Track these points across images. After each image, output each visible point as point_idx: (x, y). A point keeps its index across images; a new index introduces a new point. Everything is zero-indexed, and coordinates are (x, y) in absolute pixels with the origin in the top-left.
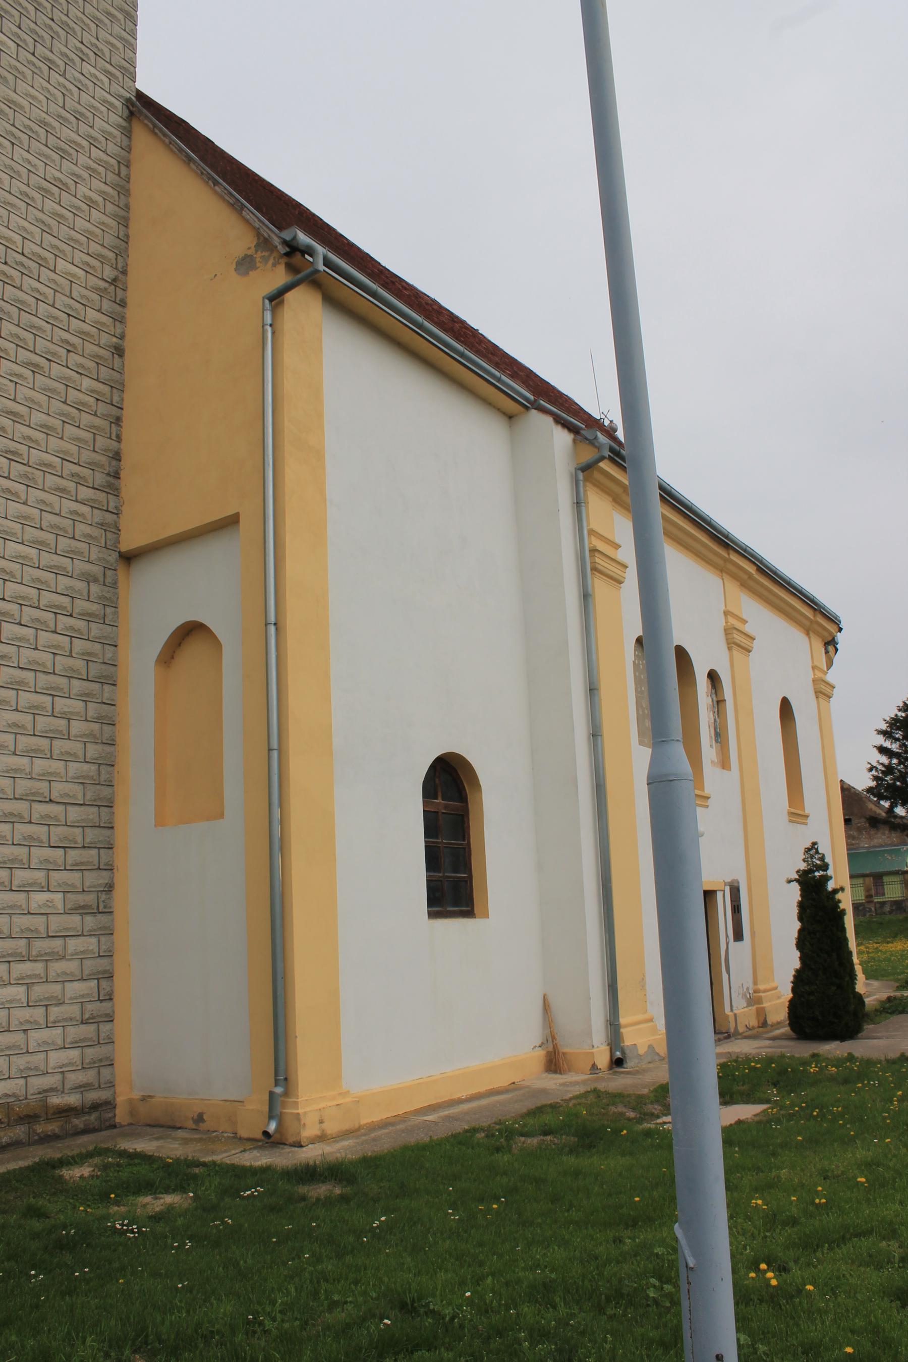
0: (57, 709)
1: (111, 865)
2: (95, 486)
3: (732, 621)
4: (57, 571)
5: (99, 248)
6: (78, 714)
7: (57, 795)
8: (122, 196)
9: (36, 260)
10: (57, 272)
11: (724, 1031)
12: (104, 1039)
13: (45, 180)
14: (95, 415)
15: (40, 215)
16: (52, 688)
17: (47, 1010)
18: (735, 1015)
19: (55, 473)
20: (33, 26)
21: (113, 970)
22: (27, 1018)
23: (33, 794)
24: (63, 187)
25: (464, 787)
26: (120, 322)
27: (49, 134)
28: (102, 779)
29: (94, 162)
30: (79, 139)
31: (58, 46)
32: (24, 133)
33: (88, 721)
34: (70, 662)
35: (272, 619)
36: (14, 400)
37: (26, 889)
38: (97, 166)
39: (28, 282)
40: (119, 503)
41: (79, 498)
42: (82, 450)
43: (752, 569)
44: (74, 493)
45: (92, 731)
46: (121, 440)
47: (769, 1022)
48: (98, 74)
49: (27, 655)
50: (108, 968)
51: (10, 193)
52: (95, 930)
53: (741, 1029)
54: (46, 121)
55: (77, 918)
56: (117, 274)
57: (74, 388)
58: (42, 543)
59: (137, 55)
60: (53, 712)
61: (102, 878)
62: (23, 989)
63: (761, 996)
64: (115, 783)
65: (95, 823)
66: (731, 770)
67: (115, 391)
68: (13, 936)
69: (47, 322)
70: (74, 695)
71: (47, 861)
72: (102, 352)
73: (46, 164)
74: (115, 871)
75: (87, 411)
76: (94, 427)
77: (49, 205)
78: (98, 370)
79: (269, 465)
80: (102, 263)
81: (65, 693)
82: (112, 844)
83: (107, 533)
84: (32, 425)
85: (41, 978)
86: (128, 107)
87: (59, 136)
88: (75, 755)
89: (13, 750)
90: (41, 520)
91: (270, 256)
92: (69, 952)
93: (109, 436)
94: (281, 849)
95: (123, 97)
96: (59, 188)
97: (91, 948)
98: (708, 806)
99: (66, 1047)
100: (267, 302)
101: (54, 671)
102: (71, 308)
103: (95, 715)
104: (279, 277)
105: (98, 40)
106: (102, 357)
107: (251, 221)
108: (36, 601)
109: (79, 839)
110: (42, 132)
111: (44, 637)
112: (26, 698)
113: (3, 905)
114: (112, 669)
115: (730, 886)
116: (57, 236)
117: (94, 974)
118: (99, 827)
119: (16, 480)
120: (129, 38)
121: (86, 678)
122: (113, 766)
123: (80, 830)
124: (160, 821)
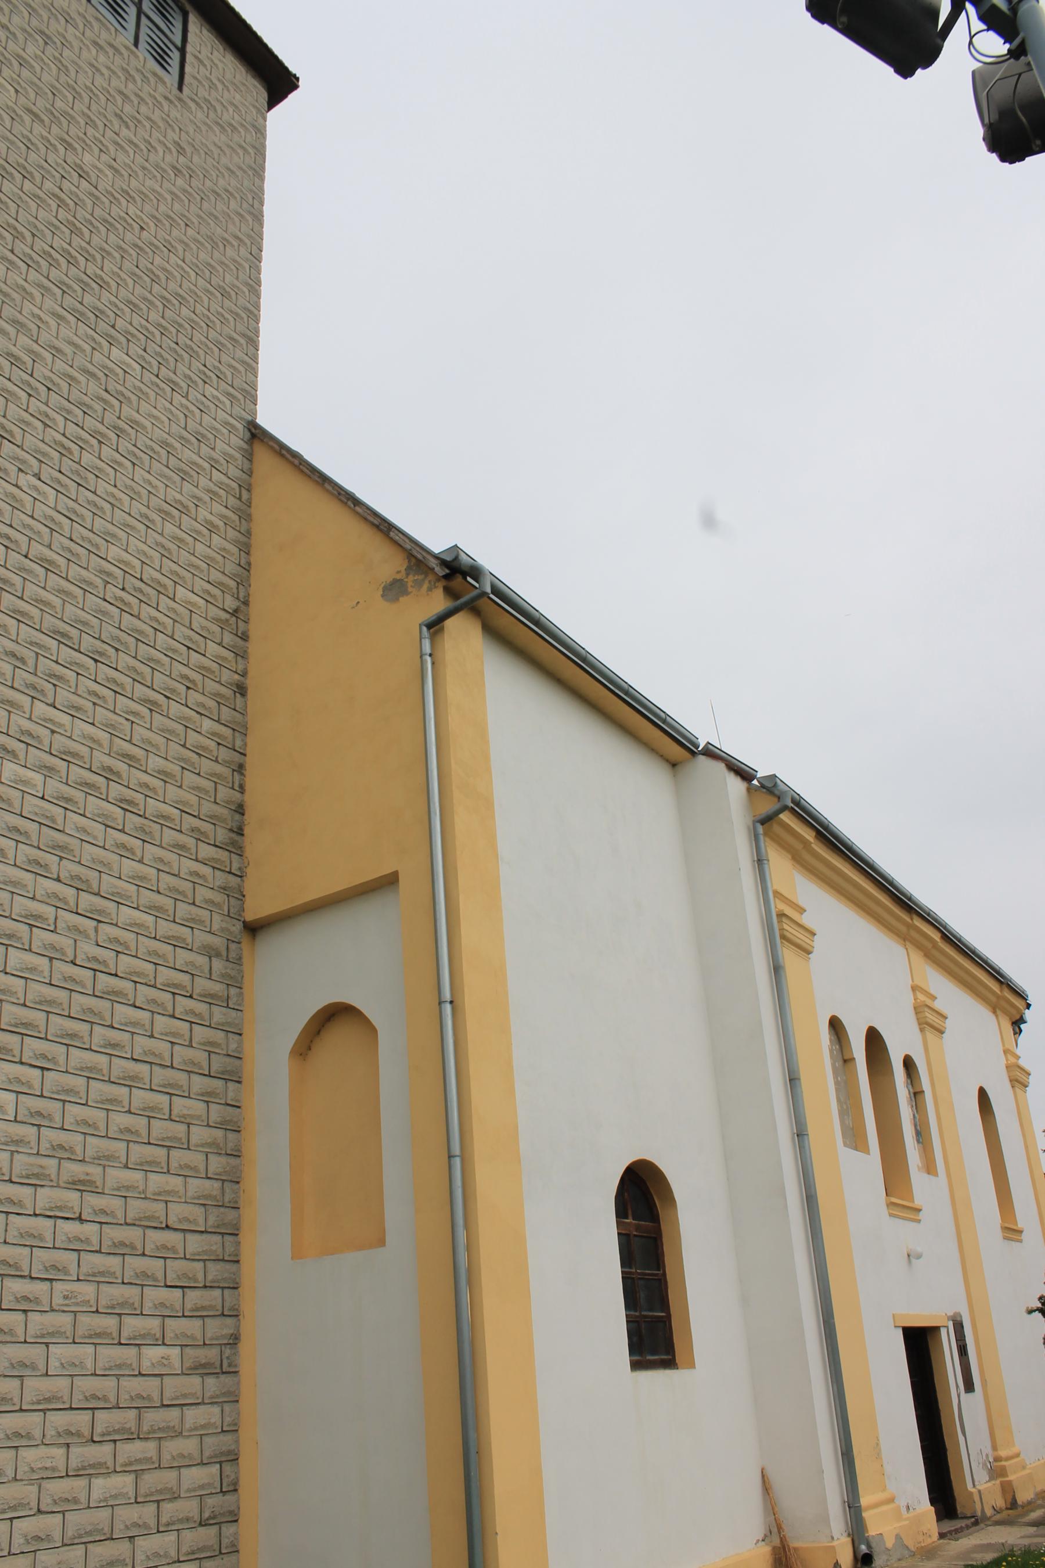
0: (175, 1112)
1: (237, 1310)
2: (217, 844)
3: (921, 997)
4: (176, 943)
5: (220, 575)
6: (199, 1117)
7: (175, 1219)
8: (243, 521)
9: (154, 586)
10: (176, 600)
11: (969, 1515)
12: (226, 1548)
13: (166, 502)
14: (217, 761)
15: (159, 538)
16: (170, 1085)
17: (158, 1507)
18: (979, 1491)
19: (173, 827)
20: (158, 349)
21: (239, 1451)
22: (135, 1520)
23: (148, 1218)
24: (184, 510)
25: (655, 1203)
26: (242, 657)
27: (170, 455)
28: (227, 1200)
29: (215, 485)
30: (200, 461)
31: (182, 368)
32: (145, 453)
33: (211, 1126)
34: (190, 1053)
35: (447, 995)
36: (130, 741)
37: (137, 1343)
38: (218, 489)
39: (147, 611)
40: (244, 863)
41: (200, 857)
42: (203, 802)
43: (936, 936)
44: (193, 851)
45: (215, 1139)
46: (245, 790)
47: (1019, 1502)
48: (220, 396)
49: (142, 1043)
50: (233, 1447)
51: (130, 514)
52: (217, 1396)
53: (989, 1512)
54: (168, 441)
55: (196, 1380)
56: (238, 604)
57: (195, 730)
58: (159, 909)
59: (259, 378)
60: (170, 1115)
61: (226, 1327)
62: (130, 1479)
63: (1005, 1466)
64: (241, 1204)
65: (218, 1255)
66: (938, 1176)
67: (237, 734)
68: (121, 1406)
69: (165, 655)
70: (195, 1094)
71: (162, 1305)
72: (223, 690)
73: (167, 486)
74: (241, 1317)
75: (207, 756)
76: (216, 774)
77: (170, 529)
78: (219, 710)
79: (436, 814)
80: (223, 592)
81: (184, 1091)
82: (237, 1283)
83: (230, 898)
84: (149, 771)
85: (153, 1463)
86: (250, 430)
87: (180, 458)
88: (195, 1169)
89: (124, 1161)
90: (158, 881)
91: (423, 580)
92: (187, 1426)
93: (231, 786)
94: (469, 1282)
95: (245, 419)
96: (179, 510)
97: (213, 1421)
98: (920, 1220)
99: (181, 1559)
100: (425, 629)
101: (172, 1064)
102: (191, 640)
103: (219, 1119)
104: (437, 602)
105: (220, 363)
106: (224, 696)
107: (401, 543)
108: (151, 977)
109: (200, 1276)
110: (163, 452)
111: (161, 1022)
112: (140, 1097)
113: (176, 1393)
114: (237, 1062)
115: (953, 1320)
116: (176, 561)
117: (216, 1456)
118: (223, 1260)
119: (131, 833)
120: (251, 362)
121: (208, 1073)
122: (238, 1183)
123: (201, 1264)
124: (298, 1253)
